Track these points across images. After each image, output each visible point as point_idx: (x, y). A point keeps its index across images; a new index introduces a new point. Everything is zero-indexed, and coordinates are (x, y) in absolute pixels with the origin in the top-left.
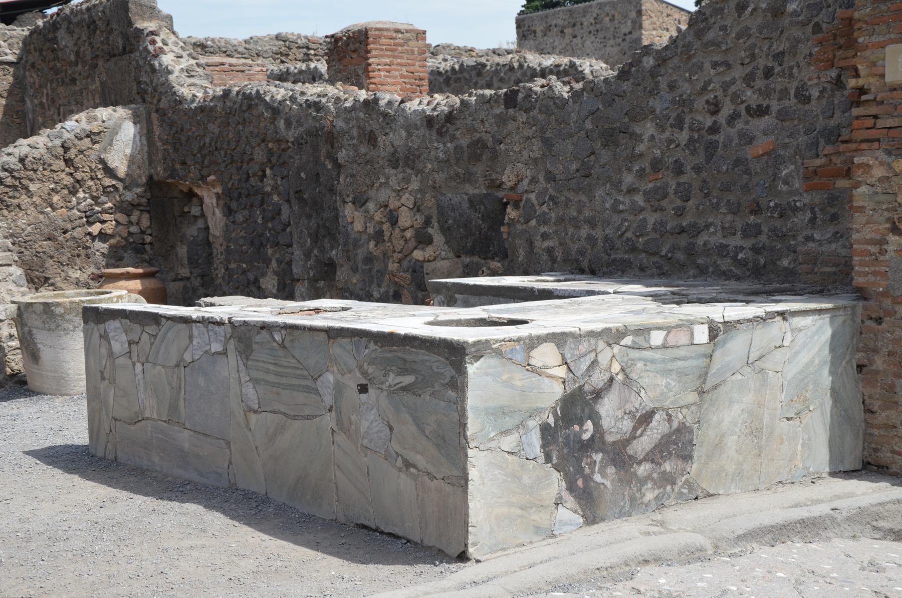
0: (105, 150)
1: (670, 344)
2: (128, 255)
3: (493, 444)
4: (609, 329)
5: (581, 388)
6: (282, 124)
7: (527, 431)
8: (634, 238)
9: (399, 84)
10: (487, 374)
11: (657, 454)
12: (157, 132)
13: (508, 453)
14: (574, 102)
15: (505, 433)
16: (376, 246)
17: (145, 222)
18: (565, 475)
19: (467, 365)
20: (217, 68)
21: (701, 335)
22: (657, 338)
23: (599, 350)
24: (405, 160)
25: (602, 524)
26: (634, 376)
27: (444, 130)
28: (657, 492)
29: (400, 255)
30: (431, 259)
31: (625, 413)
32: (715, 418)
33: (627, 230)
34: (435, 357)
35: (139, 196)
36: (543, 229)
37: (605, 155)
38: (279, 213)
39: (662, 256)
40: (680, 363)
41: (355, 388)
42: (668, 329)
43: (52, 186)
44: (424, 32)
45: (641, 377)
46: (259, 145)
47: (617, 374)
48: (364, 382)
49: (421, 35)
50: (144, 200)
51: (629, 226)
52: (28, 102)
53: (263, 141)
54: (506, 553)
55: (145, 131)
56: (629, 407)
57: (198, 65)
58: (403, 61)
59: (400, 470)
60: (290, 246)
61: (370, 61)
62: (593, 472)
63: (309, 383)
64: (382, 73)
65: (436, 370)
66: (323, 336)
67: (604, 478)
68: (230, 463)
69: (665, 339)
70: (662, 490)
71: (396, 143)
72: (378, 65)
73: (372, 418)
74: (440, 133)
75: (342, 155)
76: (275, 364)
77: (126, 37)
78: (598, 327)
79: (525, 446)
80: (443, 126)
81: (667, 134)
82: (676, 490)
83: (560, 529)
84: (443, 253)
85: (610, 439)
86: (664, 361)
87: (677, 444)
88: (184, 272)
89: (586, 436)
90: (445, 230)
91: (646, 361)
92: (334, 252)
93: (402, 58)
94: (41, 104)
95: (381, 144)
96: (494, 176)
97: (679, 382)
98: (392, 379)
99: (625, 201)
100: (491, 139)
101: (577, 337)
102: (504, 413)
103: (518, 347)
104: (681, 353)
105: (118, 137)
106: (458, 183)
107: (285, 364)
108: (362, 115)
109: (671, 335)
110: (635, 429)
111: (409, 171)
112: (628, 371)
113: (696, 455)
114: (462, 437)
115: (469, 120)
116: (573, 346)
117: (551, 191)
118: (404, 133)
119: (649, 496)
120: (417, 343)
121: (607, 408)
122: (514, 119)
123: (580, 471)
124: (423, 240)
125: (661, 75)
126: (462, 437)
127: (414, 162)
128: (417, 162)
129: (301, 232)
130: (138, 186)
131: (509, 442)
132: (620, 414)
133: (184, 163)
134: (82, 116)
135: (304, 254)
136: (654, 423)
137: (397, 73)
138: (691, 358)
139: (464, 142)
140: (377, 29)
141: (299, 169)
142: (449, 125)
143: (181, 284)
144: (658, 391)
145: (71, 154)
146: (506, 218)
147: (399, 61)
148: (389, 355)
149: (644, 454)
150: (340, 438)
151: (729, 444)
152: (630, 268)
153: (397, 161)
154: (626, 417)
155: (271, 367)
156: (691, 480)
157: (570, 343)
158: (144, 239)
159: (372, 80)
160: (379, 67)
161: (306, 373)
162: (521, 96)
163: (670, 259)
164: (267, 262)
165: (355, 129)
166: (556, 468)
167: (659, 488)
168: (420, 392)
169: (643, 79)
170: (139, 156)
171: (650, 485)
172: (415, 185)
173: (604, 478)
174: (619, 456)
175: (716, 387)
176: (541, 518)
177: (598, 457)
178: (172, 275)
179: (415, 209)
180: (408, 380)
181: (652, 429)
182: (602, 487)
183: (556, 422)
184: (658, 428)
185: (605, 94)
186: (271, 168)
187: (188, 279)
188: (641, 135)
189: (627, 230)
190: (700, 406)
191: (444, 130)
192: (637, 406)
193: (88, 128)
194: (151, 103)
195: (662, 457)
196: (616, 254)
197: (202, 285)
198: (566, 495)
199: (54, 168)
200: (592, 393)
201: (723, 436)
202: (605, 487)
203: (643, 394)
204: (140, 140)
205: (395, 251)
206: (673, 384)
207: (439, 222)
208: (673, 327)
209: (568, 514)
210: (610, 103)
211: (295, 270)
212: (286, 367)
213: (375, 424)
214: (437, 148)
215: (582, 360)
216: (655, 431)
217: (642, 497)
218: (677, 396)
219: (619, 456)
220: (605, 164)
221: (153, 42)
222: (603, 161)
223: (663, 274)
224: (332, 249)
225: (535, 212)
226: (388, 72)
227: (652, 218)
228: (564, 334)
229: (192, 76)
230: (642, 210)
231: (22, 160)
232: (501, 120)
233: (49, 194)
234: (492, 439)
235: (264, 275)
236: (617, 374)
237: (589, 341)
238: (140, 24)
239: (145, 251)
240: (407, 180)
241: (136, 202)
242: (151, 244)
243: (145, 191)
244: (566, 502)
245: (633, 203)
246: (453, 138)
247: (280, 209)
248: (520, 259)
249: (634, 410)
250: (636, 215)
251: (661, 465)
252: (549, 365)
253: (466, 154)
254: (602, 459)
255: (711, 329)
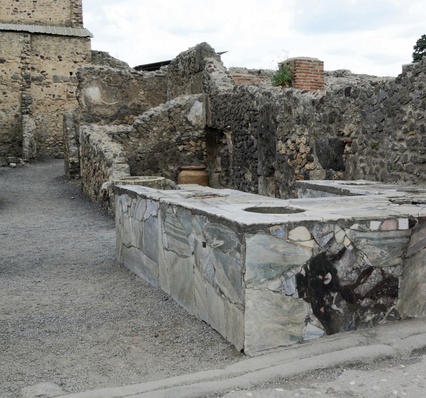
0: (186, 113)
1: (383, 229)
2: (195, 160)
3: (263, 286)
4: (343, 220)
5: (324, 253)
6: (255, 103)
7: (287, 278)
8: (402, 164)
9: (310, 85)
10: (259, 244)
11: (373, 294)
12: (210, 105)
13: (274, 291)
14: (376, 94)
15: (272, 279)
16: (290, 161)
17: (204, 145)
18: (312, 305)
19: (246, 238)
20: (237, 78)
21: (404, 224)
22: (375, 225)
23: (336, 231)
24: (303, 121)
25: (336, 334)
26: (359, 247)
27: (319, 106)
28: (374, 316)
29: (300, 166)
30: (313, 169)
31: (353, 269)
32: (413, 273)
33: (398, 160)
34: (231, 232)
35: (201, 134)
36: (361, 157)
37: (389, 121)
38: (253, 144)
39: (415, 174)
40: (390, 241)
41: (201, 244)
42: (382, 220)
43: (163, 128)
44: (323, 62)
45: (364, 248)
46: (246, 112)
47: (348, 246)
48: (205, 242)
49: (321, 64)
50: (204, 136)
51: (399, 158)
52: (168, 93)
53: (248, 110)
54: (270, 351)
55: (205, 105)
56: (356, 265)
57: (229, 77)
58: (312, 75)
59: (218, 295)
60: (257, 159)
61: (296, 74)
62: (331, 304)
63: (185, 237)
64: (302, 80)
65: (232, 239)
66: (190, 213)
67: (339, 308)
68: (159, 275)
69: (380, 227)
70: (377, 314)
71: (300, 112)
72: (300, 76)
73: (207, 262)
74: (318, 108)
75: (278, 117)
76: (174, 225)
77: (200, 65)
78: (335, 218)
79: (286, 287)
80: (319, 105)
81: (418, 111)
82: (387, 314)
83: (308, 337)
84: (318, 166)
85: (343, 284)
86: (379, 239)
87: (387, 288)
88: (220, 169)
89: (327, 282)
90: (319, 155)
91: (367, 238)
92: (274, 163)
93: (311, 73)
94: (172, 94)
95: (293, 112)
96: (340, 130)
97: (390, 251)
98: (215, 242)
99: (398, 145)
100: (339, 112)
101: (322, 224)
102: (271, 267)
103: (281, 229)
104: (392, 234)
105: (193, 108)
106: (325, 133)
107: (177, 226)
108: (286, 99)
109: (384, 224)
110: (360, 278)
111: (304, 126)
112: (355, 244)
113: (400, 294)
114: (242, 281)
115: (330, 102)
116: (318, 229)
117: (365, 138)
118: (302, 108)
119: (369, 318)
120: (224, 222)
121: (342, 266)
122: (349, 102)
123: (322, 303)
124: (310, 160)
125: (415, 81)
126: (242, 281)
127: (306, 121)
128: (308, 122)
129: (261, 153)
130: (201, 129)
131: (274, 285)
132: (350, 269)
133: (219, 120)
134: (178, 98)
135: (262, 164)
136: (372, 275)
137: (309, 81)
138: (397, 237)
139: (327, 113)
140: (299, 60)
141: (262, 123)
142: (321, 104)
143: (218, 174)
144: (375, 257)
145: (172, 114)
146: (345, 151)
147: (310, 75)
148: (214, 227)
149: (365, 293)
150: (196, 270)
151: (421, 288)
152: (400, 179)
153: (300, 120)
154: (354, 271)
155: (172, 227)
156: (396, 309)
157: (316, 227)
158: (203, 153)
159: (296, 83)
160: (300, 77)
161: (184, 232)
162: (352, 90)
163: (418, 176)
164: (248, 166)
165: (283, 105)
166: (306, 300)
167: (375, 313)
168: (225, 251)
169: (407, 83)
170: (202, 116)
171: (369, 312)
172: (306, 133)
173: (339, 308)
174: (349, 295)
175: (413, 255)
176: (295, 330)
177: (335, 295)
178: (215, 170)
179: (307, 144)
180: (221, 243)
181: (371, 279)
182: (337, 312)
183: (306, 273)
184: (375, 278)
185: (390, 90)
186: (251, 123)
187: (221, 172)
188: (406, 111)
189: (398, 160)
190: (403, 266)
191: (319, 106)
192: (361, 265)
193: (180, 103)
194: (208, 93)
195: (377, 295)
196: (393, 172)
197: (226, 175)
198: (312, 317)
199: (164, 120)
200: (331, 257)
201: (417, 283)
202: (339, 312)
203: (365, 258)
204: (203, 109)
205: (298, 164)
206: (385, 252)
207: (316, 151)
208: (386, 219)
209: (314, 328)
210: (391, 95)
211: (258, 171)
212: (177, 227)
213: (209, 266)
214: (316, 115)
215: (324, 237)
216: (373, 280)
217: (363, 319)
218: (388, 260)
219: (349, 295)
220: (389, 126)
221: (210, 66)
222: (388, 124)
223: (415, 184)
224: (273, 161)
225: (358, 148)
226: (305, 79)
227: (410, 155)
228: (312, 222)
229: (225, 81)
230: (406, 150)
231: (151, 116)
232: (344, 102)
233: (161, 132)
234: (263, 283)
235: (246, 172)
236: (348, 246)
237: (329, 226)
238: (206, 59)
239: (203, 159)
240: (303, 130)
241: (200, 136)
242: (206, 155)
243: (204, 132)
244: (312, 321)
245: (402, 146)
246: (323, 111)
247: (253, 142)
248: (351, 171)
249: (359, 267)
250: (403, 152)
251: (377, 300)
252: (302, 240)
253: (328, 118)
254: (338, 296)
255: (410, 221)
